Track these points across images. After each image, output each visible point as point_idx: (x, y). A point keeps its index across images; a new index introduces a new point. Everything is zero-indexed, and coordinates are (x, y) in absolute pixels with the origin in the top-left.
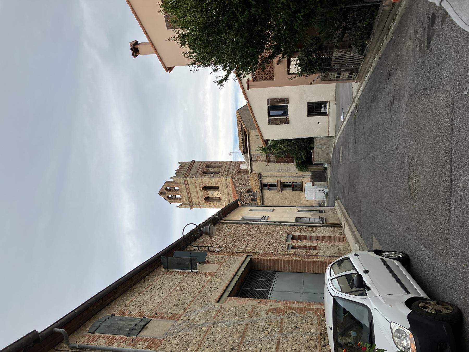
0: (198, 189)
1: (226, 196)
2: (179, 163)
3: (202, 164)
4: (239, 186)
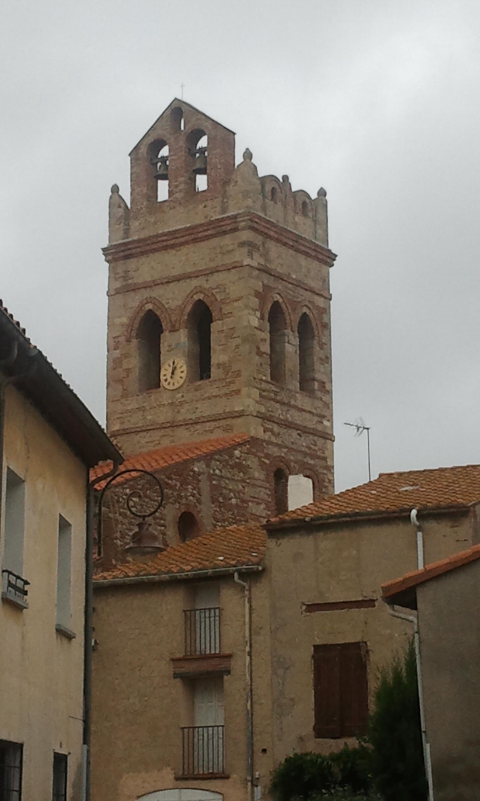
0: (195, 283)
1: (164, 416)
2: (322, 193)
3: (320, 302)
4: (211, 477)
